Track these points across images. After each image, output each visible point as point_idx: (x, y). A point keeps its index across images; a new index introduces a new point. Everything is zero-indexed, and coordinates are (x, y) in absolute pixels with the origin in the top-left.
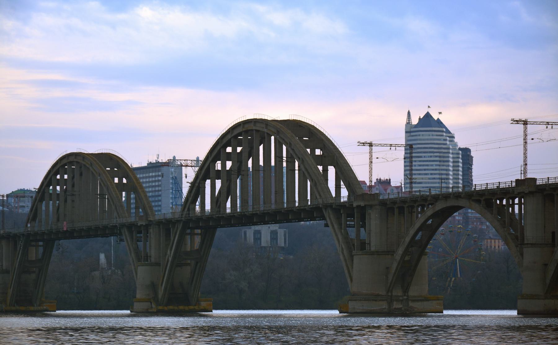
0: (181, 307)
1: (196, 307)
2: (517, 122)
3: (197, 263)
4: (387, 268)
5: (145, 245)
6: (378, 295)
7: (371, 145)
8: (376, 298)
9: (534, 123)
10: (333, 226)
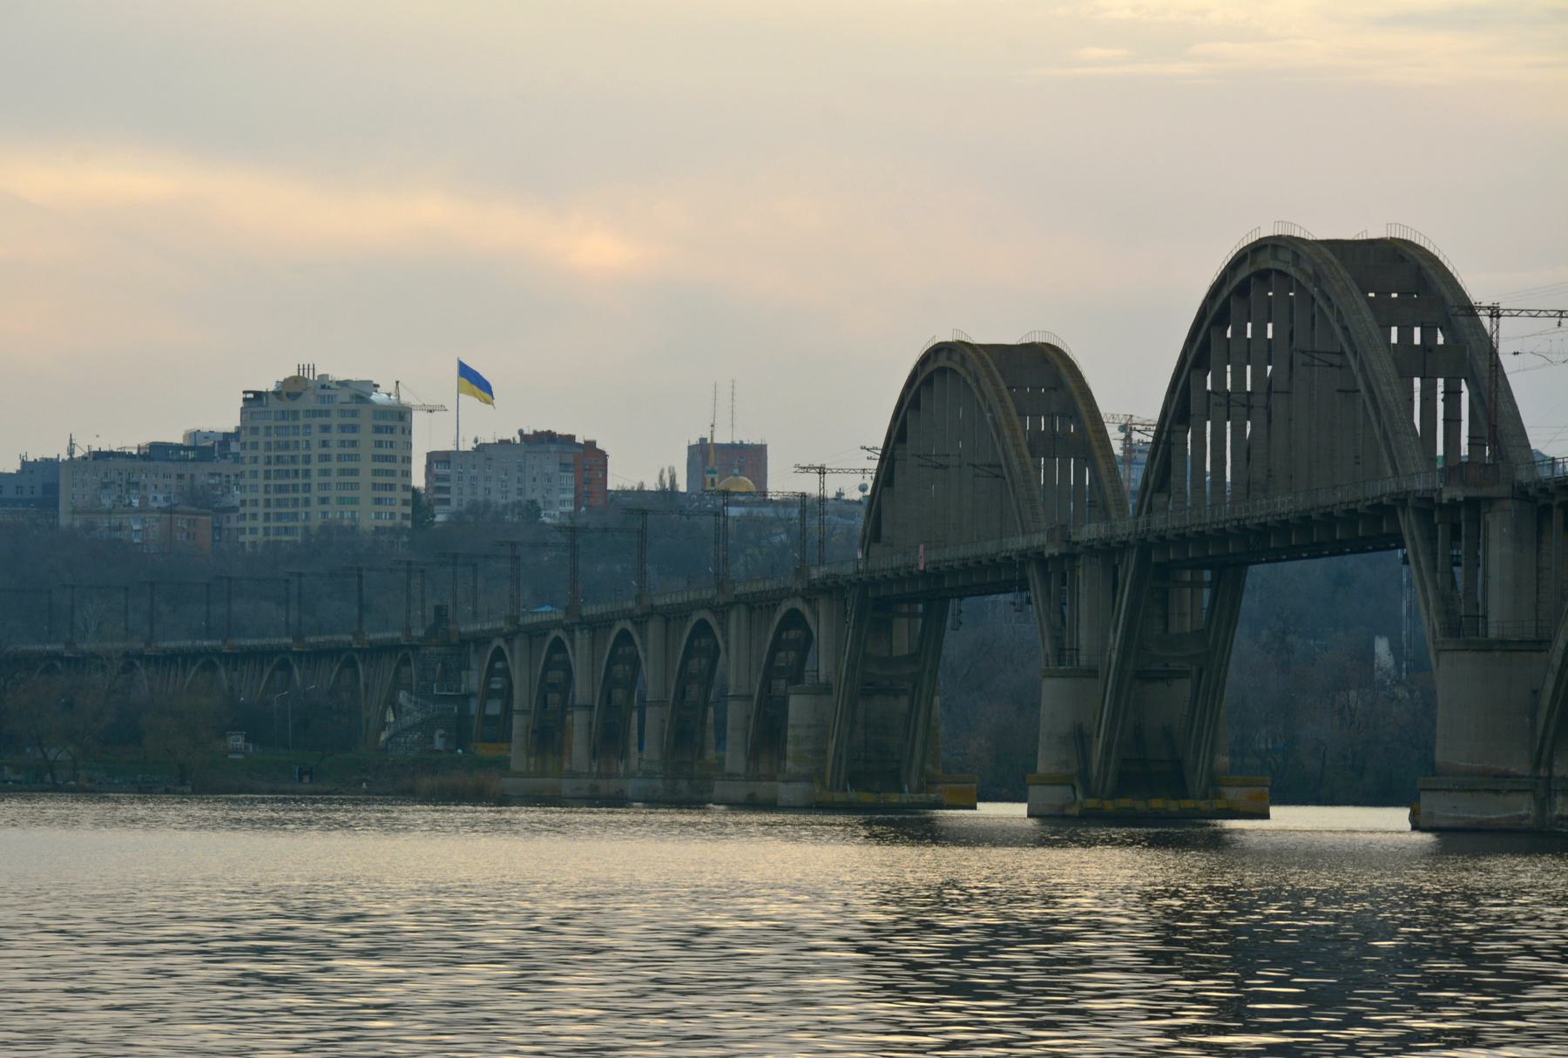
0: (1157, 804)
1: (1202, 804)
2: (806, 469)
3: (1201, 670)
4: (1535, 692)
5: (1471, 578)
6: (1506, 775)
7: (822, 471)
8: (1496, 783)
9: (1515, 313)
10: (1418, 562)
